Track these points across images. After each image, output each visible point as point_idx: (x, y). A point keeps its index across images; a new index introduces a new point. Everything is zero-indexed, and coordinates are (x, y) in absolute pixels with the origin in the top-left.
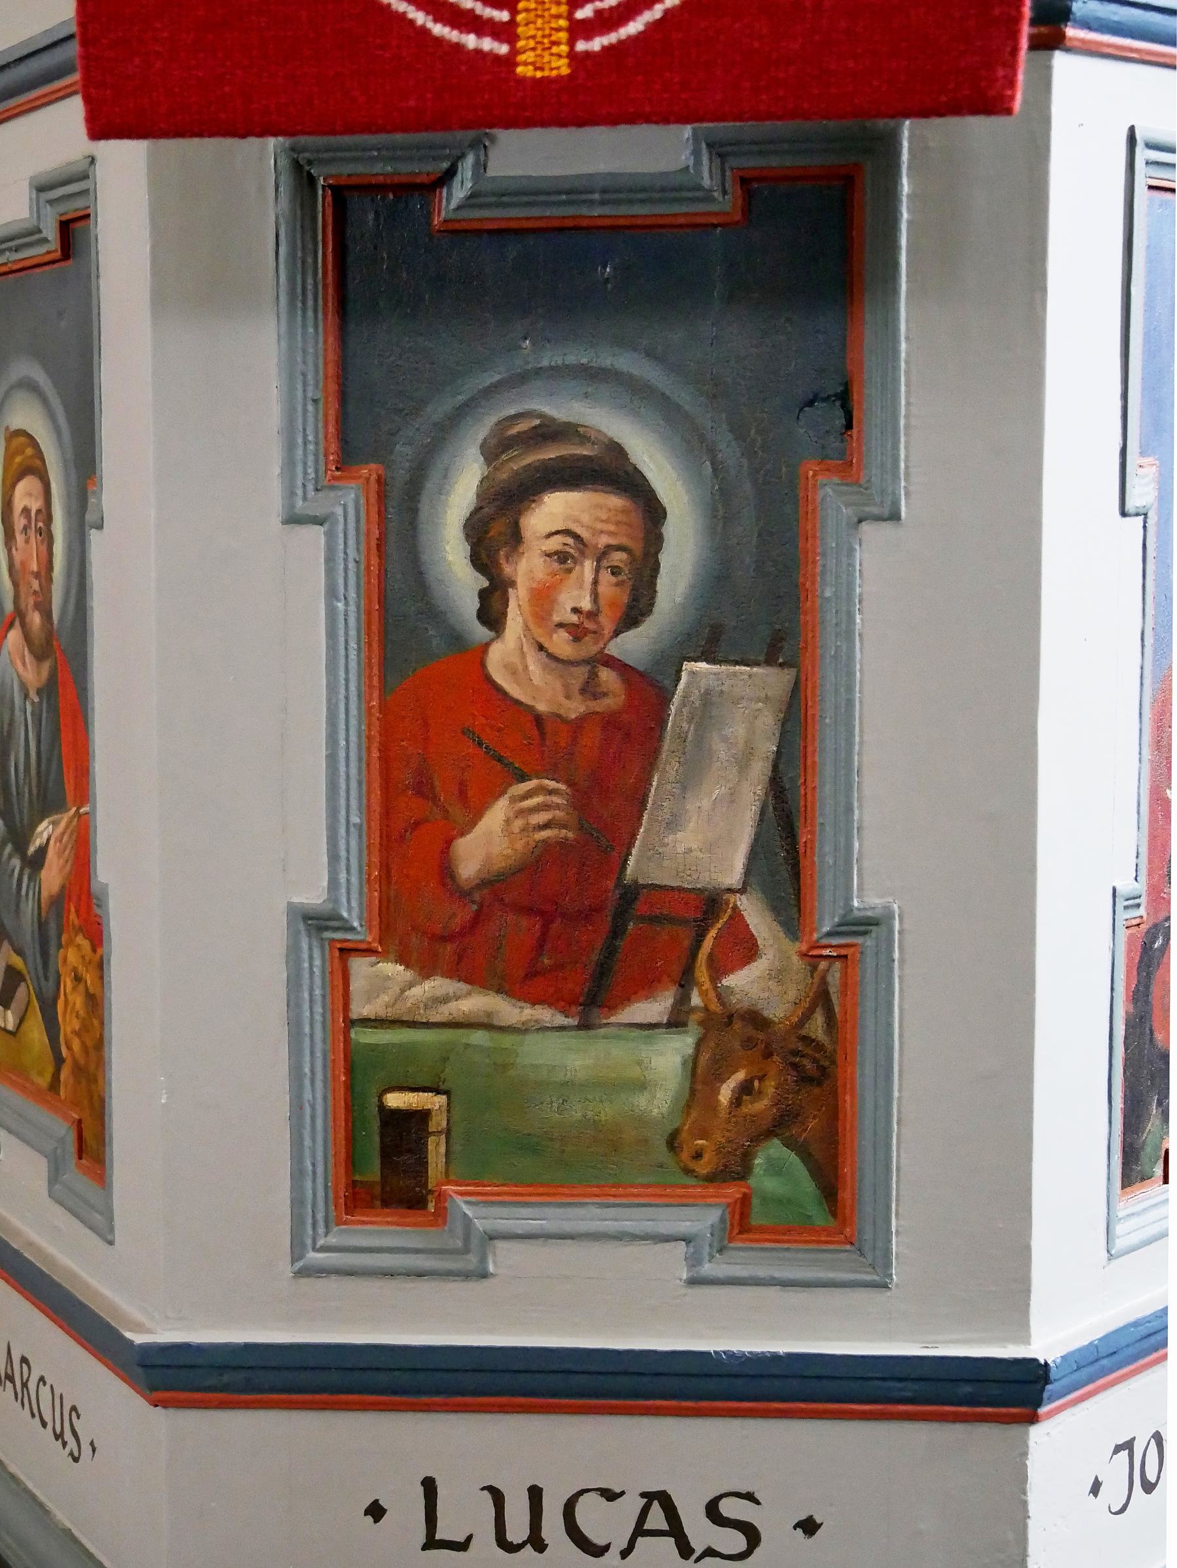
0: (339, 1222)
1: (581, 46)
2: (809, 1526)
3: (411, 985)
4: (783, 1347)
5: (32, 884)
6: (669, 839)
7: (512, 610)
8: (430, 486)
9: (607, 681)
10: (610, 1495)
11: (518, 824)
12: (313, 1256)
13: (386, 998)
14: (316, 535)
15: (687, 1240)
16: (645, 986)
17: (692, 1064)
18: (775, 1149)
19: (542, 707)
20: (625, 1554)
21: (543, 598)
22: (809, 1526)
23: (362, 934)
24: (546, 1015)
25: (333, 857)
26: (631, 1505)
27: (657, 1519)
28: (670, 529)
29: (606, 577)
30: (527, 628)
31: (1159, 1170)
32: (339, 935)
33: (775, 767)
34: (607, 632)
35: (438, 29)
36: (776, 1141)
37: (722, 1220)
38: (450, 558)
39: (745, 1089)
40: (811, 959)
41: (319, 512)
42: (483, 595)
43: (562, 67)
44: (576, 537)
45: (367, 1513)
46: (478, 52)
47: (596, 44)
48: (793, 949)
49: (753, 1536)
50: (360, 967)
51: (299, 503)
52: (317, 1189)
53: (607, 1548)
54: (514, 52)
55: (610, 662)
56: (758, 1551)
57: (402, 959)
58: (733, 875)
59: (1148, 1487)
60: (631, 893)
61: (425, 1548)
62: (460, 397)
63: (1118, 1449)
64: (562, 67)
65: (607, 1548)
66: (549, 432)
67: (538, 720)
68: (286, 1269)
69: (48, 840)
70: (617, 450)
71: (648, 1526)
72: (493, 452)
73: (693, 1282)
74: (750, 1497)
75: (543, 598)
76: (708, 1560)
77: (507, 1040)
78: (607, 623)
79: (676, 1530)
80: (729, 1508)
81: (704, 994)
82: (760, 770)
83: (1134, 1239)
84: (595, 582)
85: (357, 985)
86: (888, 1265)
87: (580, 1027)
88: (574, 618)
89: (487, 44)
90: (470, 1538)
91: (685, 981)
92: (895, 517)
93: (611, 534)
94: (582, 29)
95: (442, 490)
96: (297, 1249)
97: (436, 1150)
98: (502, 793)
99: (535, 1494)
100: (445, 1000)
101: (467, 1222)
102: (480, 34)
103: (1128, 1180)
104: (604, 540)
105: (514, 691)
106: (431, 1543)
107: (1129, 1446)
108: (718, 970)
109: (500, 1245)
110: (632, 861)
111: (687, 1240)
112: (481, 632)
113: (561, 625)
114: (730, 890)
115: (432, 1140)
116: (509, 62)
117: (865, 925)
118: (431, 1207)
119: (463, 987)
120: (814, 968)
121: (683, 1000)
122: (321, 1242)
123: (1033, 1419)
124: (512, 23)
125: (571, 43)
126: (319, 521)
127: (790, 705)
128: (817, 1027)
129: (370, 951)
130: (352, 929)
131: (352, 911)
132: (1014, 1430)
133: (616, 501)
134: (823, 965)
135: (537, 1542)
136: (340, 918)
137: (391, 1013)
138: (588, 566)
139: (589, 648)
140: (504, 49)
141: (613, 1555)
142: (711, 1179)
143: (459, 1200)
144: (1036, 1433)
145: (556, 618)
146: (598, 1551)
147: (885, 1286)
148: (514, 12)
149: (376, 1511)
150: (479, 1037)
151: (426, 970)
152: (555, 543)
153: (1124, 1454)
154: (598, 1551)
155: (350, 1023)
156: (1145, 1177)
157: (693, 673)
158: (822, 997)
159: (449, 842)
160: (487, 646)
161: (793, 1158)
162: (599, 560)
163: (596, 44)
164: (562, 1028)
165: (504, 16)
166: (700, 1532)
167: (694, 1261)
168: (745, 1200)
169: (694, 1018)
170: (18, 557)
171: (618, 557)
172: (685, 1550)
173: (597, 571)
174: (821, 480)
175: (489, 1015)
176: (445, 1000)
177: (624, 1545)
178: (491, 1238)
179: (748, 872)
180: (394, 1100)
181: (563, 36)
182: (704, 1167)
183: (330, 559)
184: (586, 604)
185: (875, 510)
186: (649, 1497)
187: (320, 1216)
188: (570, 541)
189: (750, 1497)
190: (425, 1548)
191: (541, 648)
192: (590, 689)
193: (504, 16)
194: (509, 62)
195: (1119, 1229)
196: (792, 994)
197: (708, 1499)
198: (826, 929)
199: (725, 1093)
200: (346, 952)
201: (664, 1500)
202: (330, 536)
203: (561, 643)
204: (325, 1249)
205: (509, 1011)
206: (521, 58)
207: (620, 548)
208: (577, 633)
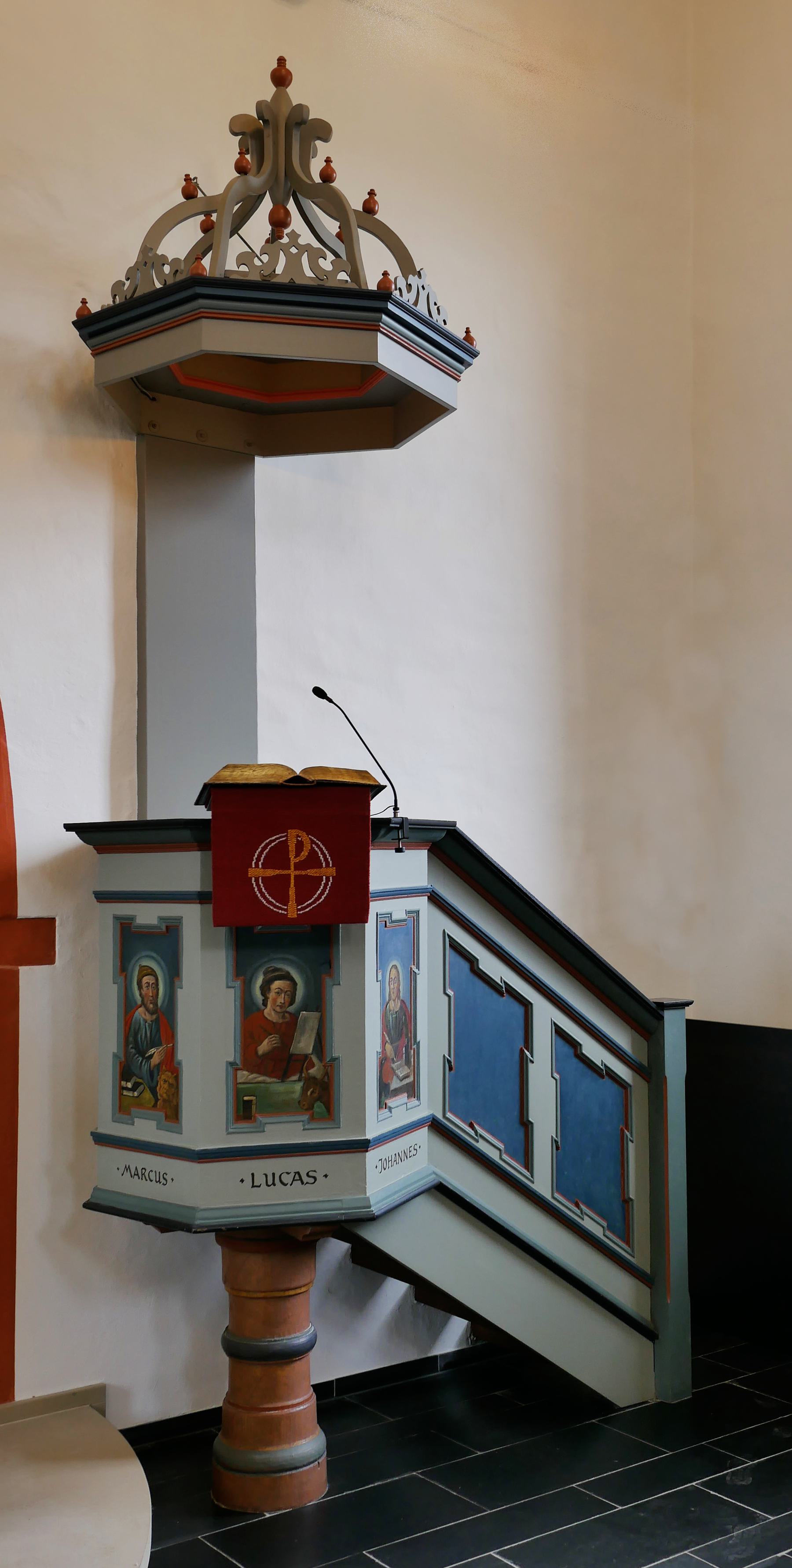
0: (235, 1123)
1: (299, 913)
2: (326, 1176)
3: (249, 1075)
4: (322, 1141)
5: (146, 1063)
6: (298, 1045)
7: (269, 1003)
10: (288, 1173)
11: (270, 1043)
12: (231, 1130)
13: (245, 1078)
14: (232, 990)
15: (303, 1121)
16: (294, 1074)
17: (303, 1088)
18: (318, 1103)
19: (274, 1021)
20: (291, 1185)
21: (275, 1000)
23: (240, 1066)
24: (275, 1080)
25: (235, 1051)
26: (292, 1175)
27: (297, 1177)
28: (298, 987)
29: (286, 996)
30: (271, 1006)
31: (384, 1107)
32: (235, 1066)
33: (318, 1030)
34: (287, 1006)
35: (275, 909)
36: (319, 1102)
37: (309, 1117)
38: (257, 993)
39: (312, 1092)
40: (325, 1066)
41: (233, 986)
42: (263, 1000)
43: (296, 916)
44: (281, 989)
46: (281, 913)
47: (301, 912)
48: (321, 1065)
49: (315, 1178)
50: (239, 1073)
51: (229, 984)
52: (231, 1117)
53: (287, 1184)
54: (287, 913)
55: (287, 1012)
56: (316, 1182)
57: (247, 1071)
58: (310, 1051)
59: (385, 1169)
60: (292, 1055)
61: (252, 1187)
63: (380, 1160)
64: (296, 916)
65: (287, 1184)
66: (276, 970)
67: (274, 1023)
68: (225, 1133)
69: (154, 1053)
70: (288, 973)
72: (265, 974)
73: (304, 1130)
74: (315, 1171)
75: (275, 1000)
76: (307, 1185)
77: (268, 1085)
78: (287, 1004)
79: (301, 1179)
80: (311, 1174)
81: (305, 1074)
82: (315, 1031)
83: (382, 1119)
84: (284, 997)
85: (238, 1076)
86: (340, 1124)
87: (282, 1082)
88: (280, 1004)
89: (283, 912)
90: (261, 1185)
91: (301, 1073)
92: (339, 984)
93: (287, 988)
94: (257, 880)
95: (256, 979)
96: (227, 1129)
97: (254, 1107)
98: (267, 1037)
99: (274, 1174)
100: (256, 1078)
101: (261, 1121)
102: (282, 910)
103: (379, 1109)
104: (286, 990)
105: (269, 1018)
106: (253, 1186)
107: (381, 1160)
108: (307, 1069)
109: (267, 1125)
110: (291, 1049)
111: (303, 1121)
112: (263, 1007)
113: (277, 1006)
114: (310, 1054)
115: (253, 1106)
116: (287, 915)
117: (337, 1059)
118: (253, 1119)
119: (259, 1075)
120: (325, 1068)
121: (301, 1075)
122: (232, 1127)
123: (367, 1151)
124: (287, 909)
125: (297, 912)
126: (233, 987)
127: (320, 1019)
128: (326, 1079)
129: (241, 1069)
130: (238, 1065)
131: (238, 1062)
132: (364, 1153)
133: (288, 982)
134: (327, 1067)
135: (274, 1184)
136: (236, 1063)
137: (245, 1081)
138: (283, 995)
139: (284, 1010)
140: (286, 913)
141: (289, 1185)
142: (307, 1110)
143: (259, 1117)
144: (367, 1154)
145: (277, 1004)
146: (285, 1185)
147: (339, 1128)
148: (287, 907)
149: (242, 1181)
150: (262, 1085)
151: (252, 1073)
152: (277, 990)
153: (380, 1161)
154: (285, 1185)
155: (237, 1084)
156: (382, 1108)
157: (302, 1014)
158: (327, 1074)
159: (256, 1047)
160: (264, 1010)
161: (322, 1104)
162: (285, 993)
163: (301, 912)
164: (279, 1082)
165: (286, 907)
166: (305, 1179)
167: (304, 1125)
168: (313, 1113)
169: (303, 1079)
170: (143, 993)
171: (289, 993)
172: (302, 1183)
173: (285, 995)
174: (326, 977)
175: (264, 1080)
176: (256, 1078)
177: (291, 1183)
178: (266, 1124)
179: (313, 1050)
180: (246, 1098)
181: (296, 911)
182: (305, 1108)
183: (235, 994)
184: (283, 1002)
185: (336, 983)
186: (295, 1173)
187: (231, 1122)
188: (279, 990)
189: (315, 1171)
190: (252, 1187)
191: (274, 1010)
192: (284, 1017)
193: (286, 907)
194: (287, 915)
195: (379, 1116)
196: (321, 1073)
198: (328, 1060)
199: (309, 1093)
200: (237, 1069)
201: (298, 1173)
202: (235, 990)
203: (278, 1009)
204: (232, 1129)
205: (268, 1079)
206: (289, 914)
207: (289, 991)
208: (281, 1007)
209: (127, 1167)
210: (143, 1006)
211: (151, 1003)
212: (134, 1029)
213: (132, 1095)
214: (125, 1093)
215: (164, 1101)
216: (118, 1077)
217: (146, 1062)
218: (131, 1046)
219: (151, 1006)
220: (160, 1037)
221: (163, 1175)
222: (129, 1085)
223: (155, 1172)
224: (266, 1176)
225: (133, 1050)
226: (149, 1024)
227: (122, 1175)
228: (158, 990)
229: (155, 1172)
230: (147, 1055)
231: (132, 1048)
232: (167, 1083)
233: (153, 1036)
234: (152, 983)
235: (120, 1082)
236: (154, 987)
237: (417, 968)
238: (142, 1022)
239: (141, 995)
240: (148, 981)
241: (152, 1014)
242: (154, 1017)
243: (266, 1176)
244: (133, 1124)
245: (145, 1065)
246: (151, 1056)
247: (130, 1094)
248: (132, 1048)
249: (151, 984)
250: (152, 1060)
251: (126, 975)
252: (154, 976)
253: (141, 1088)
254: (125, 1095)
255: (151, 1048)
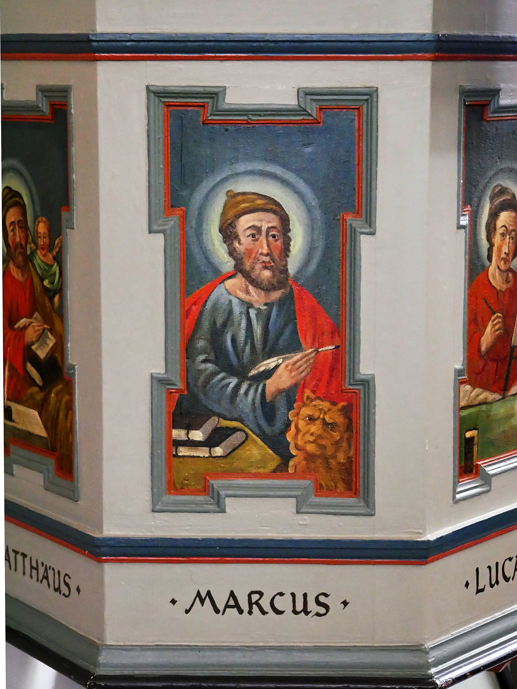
8: (480, 213)
9: (240, 394)
22: (173, 602)
27: (232, 602)
45: (176, 601)
49: (327, 607)
62: (486, 180)
71: (229, 604)
80: (322, 599)
99: (305, 595)
112: (487, 263)
115: (475, 446)
184: (507, 251)
197: (264, 596)
208: (506, 260)
209: (203, 595)
210: (239, 275)
211: (266, 268)
212: (214, 323)
213: (207, 455)
214: (183, 451)
215: (310, 457)
216: (164, 420)
217: (250, 386)
218: (202, 357)
219: (267, 274)
220: (295, 332)
221: (65, 577)
222: (197, 435)
223: (293, 595)
224: (489, 567)
225: (210, 367)
226: (259, 310)
227: (187, 612)
228: (287, 242)
229: (293, 595)
230: (253, 372)
231: (205, 361)
232: (318, 422)
233: (272, 335)
234: (269, 228)
235: (171, 432)
236: (274, 236)
237: (366, 221)
238: (237, 309)
239: (232, 253)
240: (258, 224)
241: (268, 289)
242: (276, 295)
243: (489, 567)
244: (223, 511)
245: (246, 393)
246: (268, 374)
247: (203, 452)
248: (205, 361)
249: (264, 229)
250: (268, 382)
251: (184, 218)
252: (274, 212)
253: (236, 438)
254: (183, 457)
255: (269, 358)
